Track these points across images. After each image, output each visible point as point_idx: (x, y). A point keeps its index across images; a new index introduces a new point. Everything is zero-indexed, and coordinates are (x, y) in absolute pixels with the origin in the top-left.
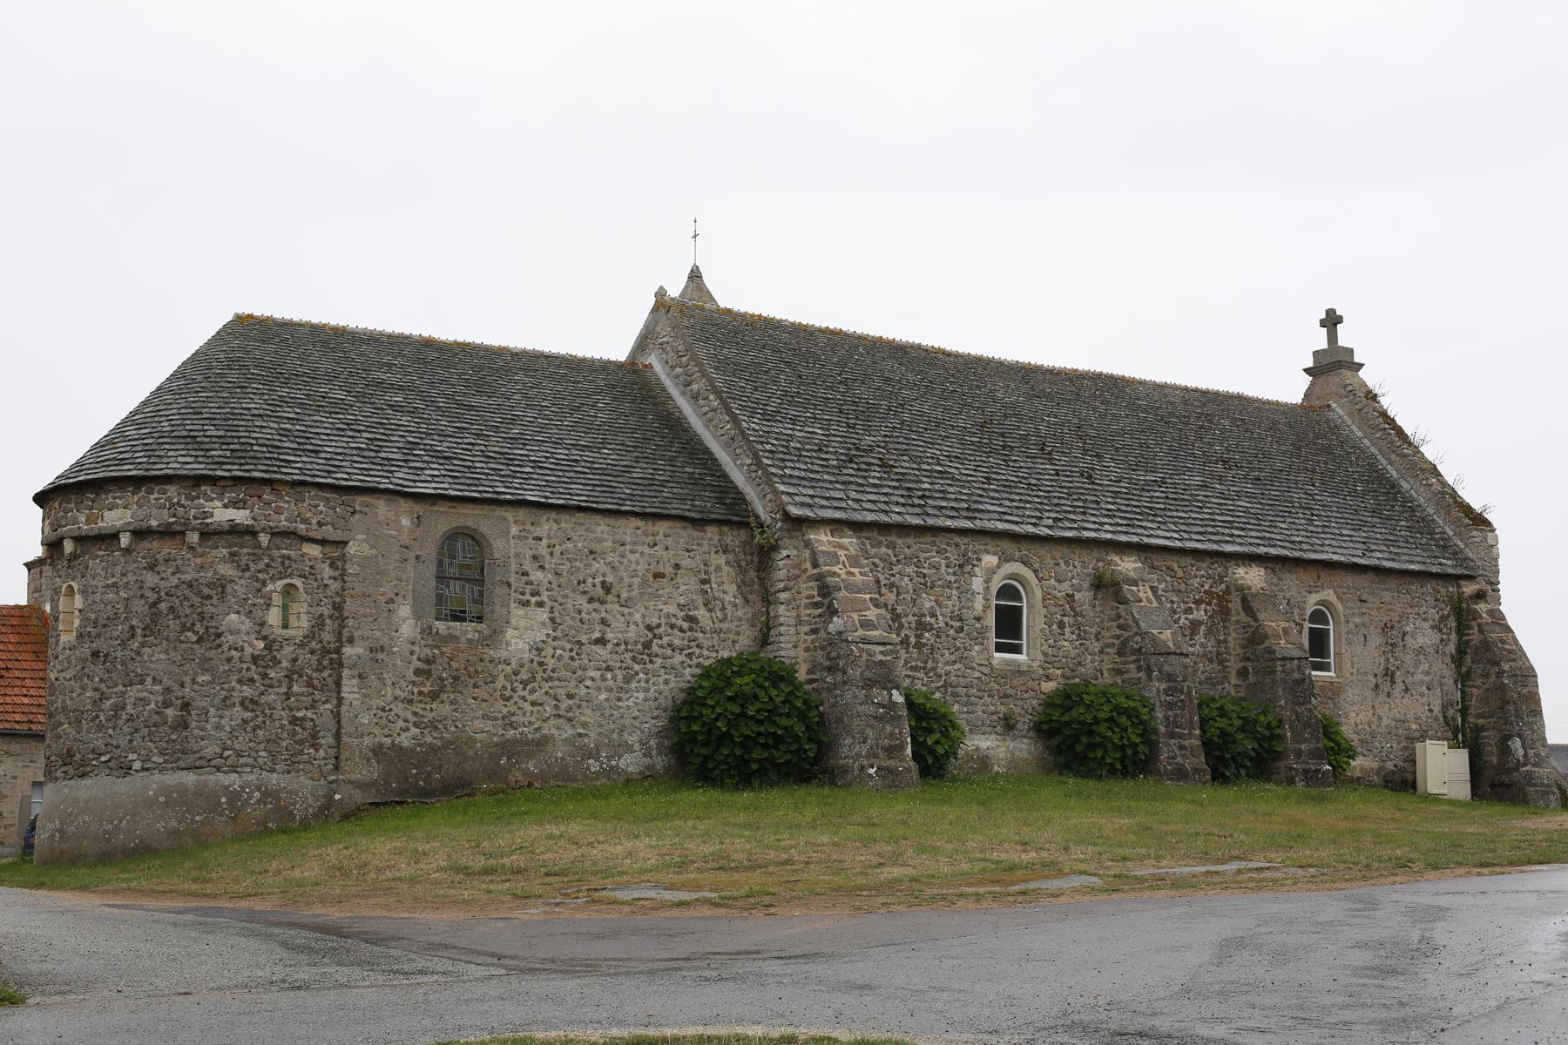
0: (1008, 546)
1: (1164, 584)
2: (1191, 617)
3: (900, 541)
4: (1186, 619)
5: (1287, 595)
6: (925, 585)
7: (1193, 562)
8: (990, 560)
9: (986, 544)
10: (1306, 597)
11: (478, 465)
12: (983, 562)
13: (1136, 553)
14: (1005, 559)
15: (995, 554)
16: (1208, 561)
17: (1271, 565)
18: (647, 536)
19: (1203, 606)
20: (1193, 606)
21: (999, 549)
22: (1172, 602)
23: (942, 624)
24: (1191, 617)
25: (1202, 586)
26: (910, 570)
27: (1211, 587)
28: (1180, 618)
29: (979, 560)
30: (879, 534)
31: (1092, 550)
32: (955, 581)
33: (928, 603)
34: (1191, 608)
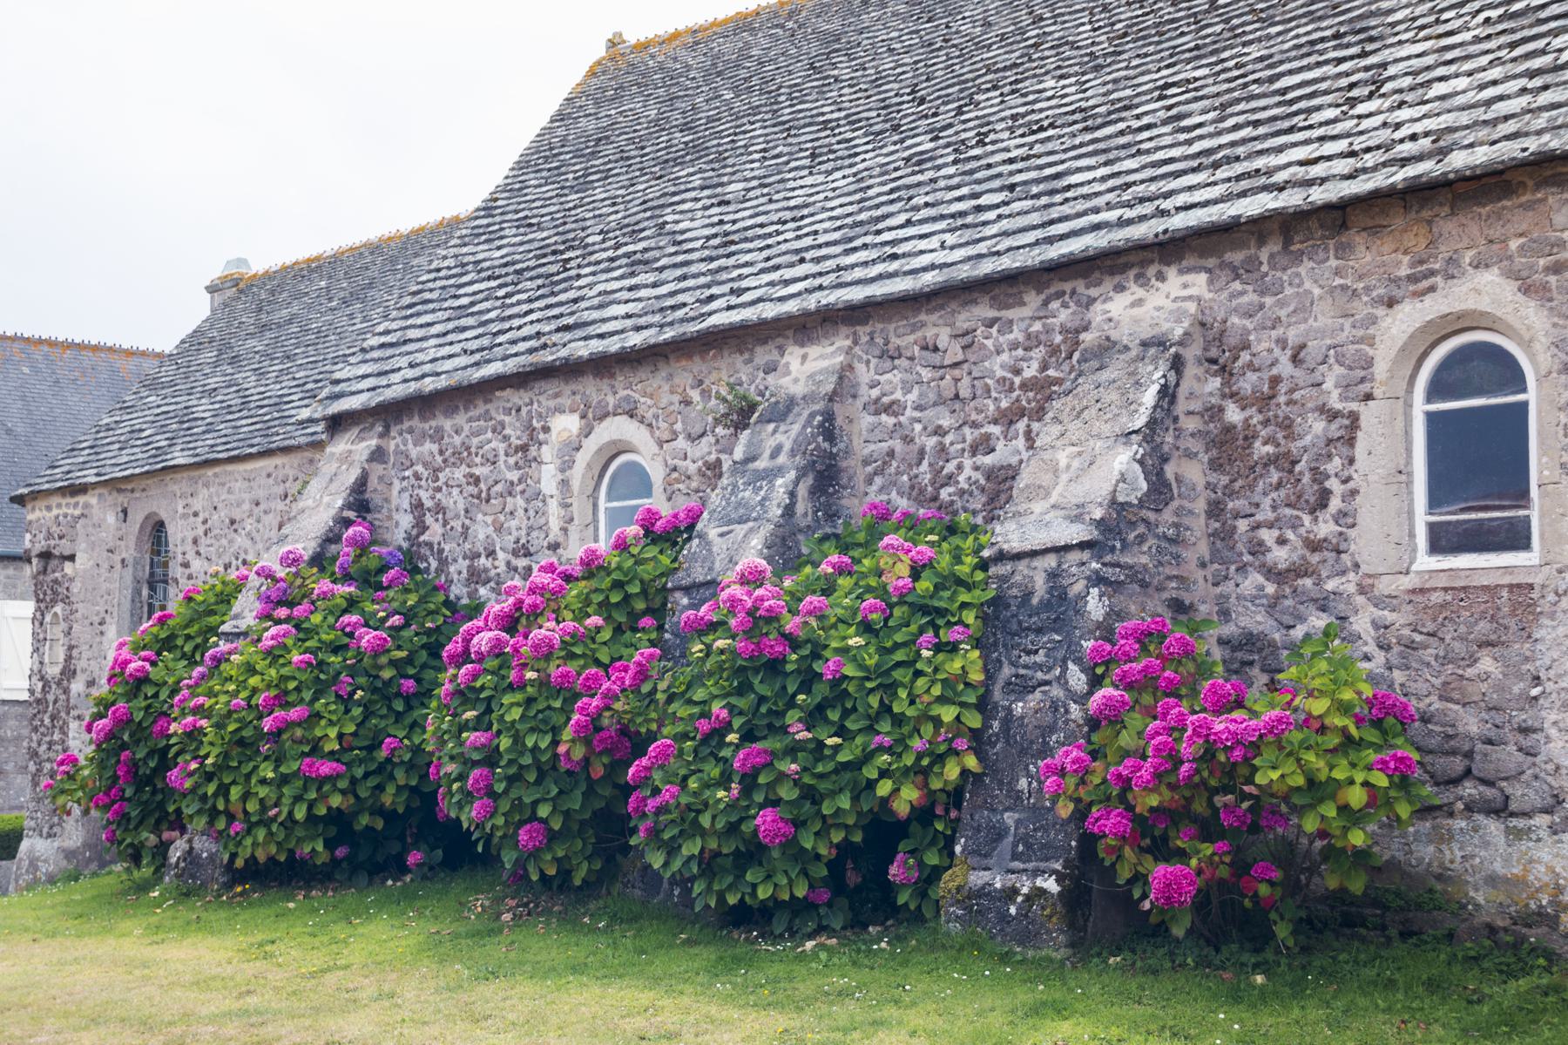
0: (591, 388)
1: (916, 391)
2: (988, 460)
3: (448, 425)
4: (977, 468)
5: (1293, 335)
6: (478, 497)
7: (992, 313)
8: (566, 424)
9: (557, 395)
10: (1373, 320)
11: (1073, 89)
12: (554, 433)
13: (844, 330)
14: (593, 416)
15: (573, 411)
16: (1033, 300)
17: (1237, 257)
18: (468, 582)
19: (1021, 426)
20: (995, 430)
21: (578, 397)
22: (939, 431)
23: (502, 568)
24: (988, 460)
25: (1017, 372)
26: (459, 473)
27: (1044, 367)
28: (960, 467)
29: (546, 429)
30: (424, 419)
31: (752, 351)
32: (520, 481)
33: (482, 531)
34: (987, 437)
